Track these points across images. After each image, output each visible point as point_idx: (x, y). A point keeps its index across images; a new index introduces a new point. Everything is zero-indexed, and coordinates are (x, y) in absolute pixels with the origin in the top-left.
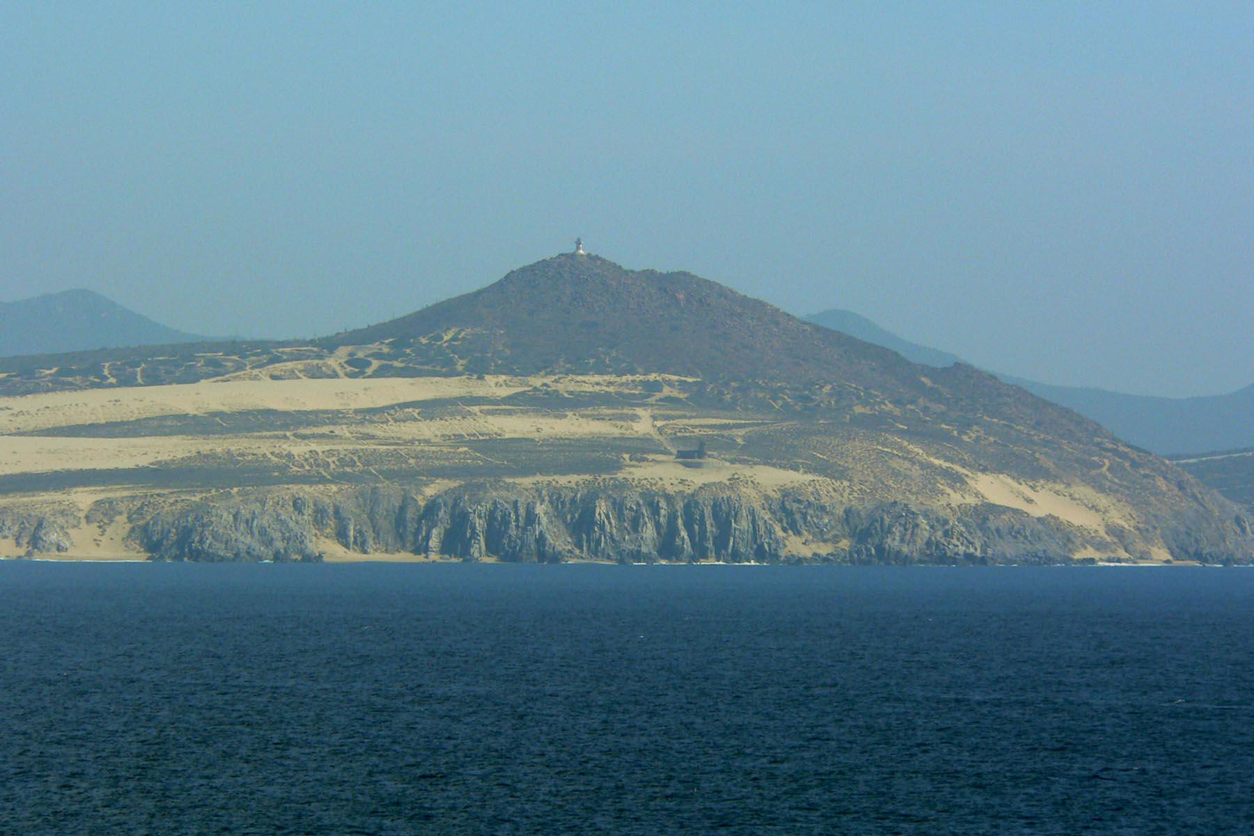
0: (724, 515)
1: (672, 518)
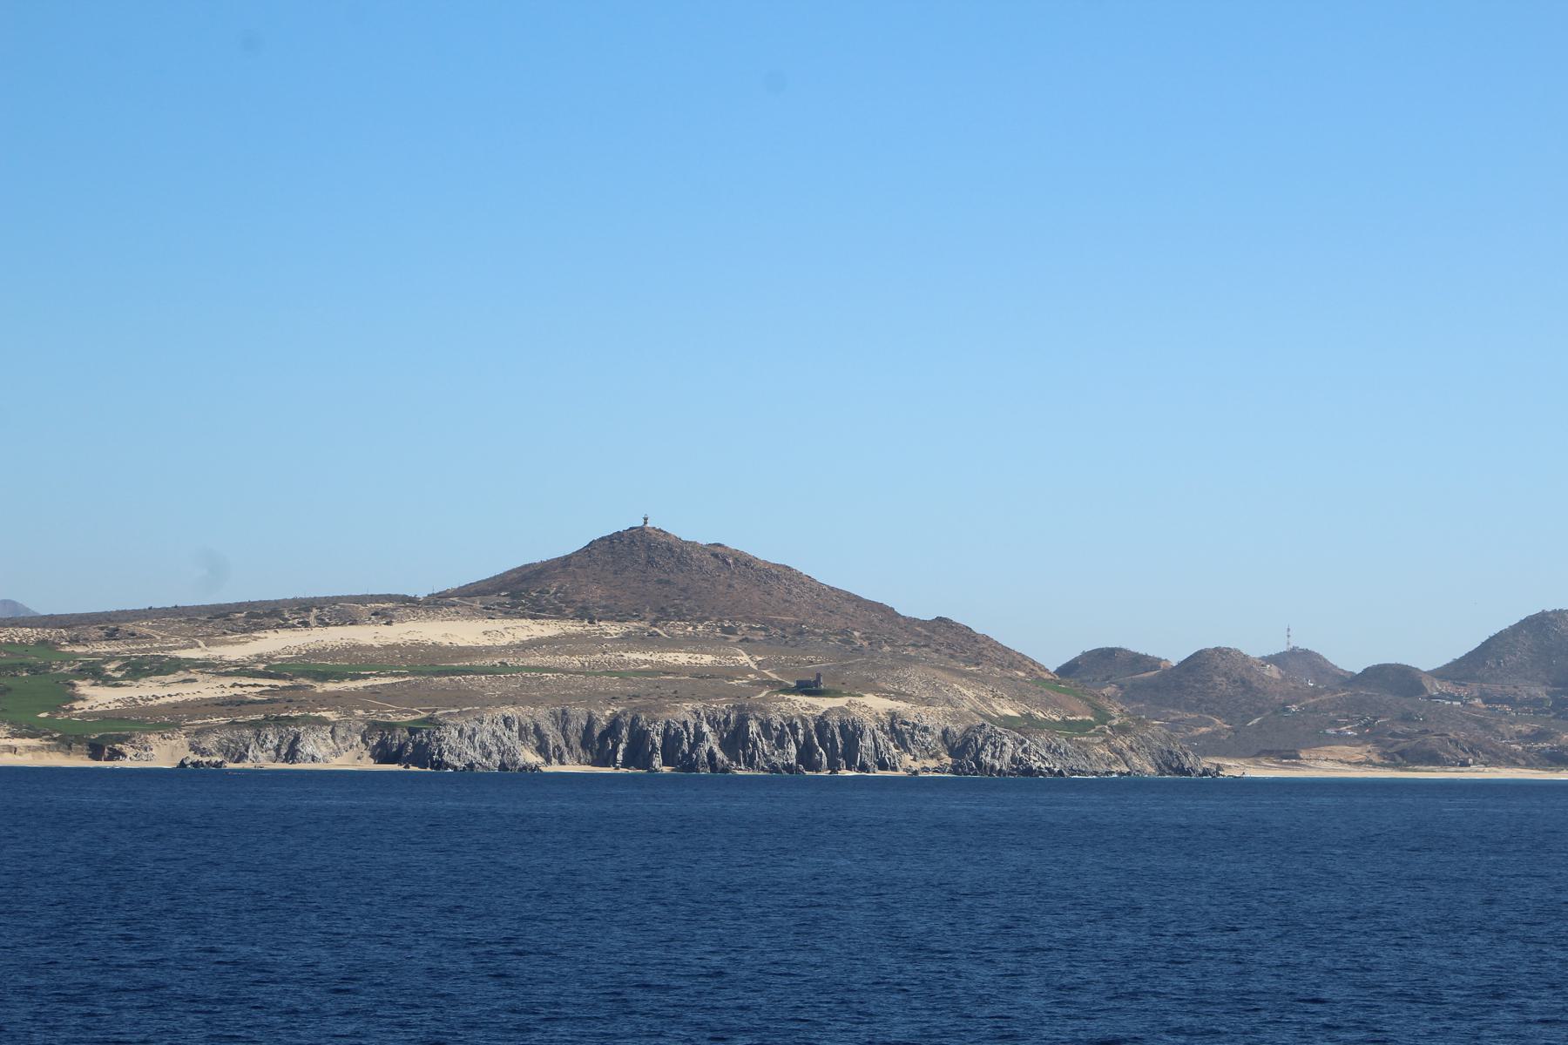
0: (852, 734)
1: (808, 735)
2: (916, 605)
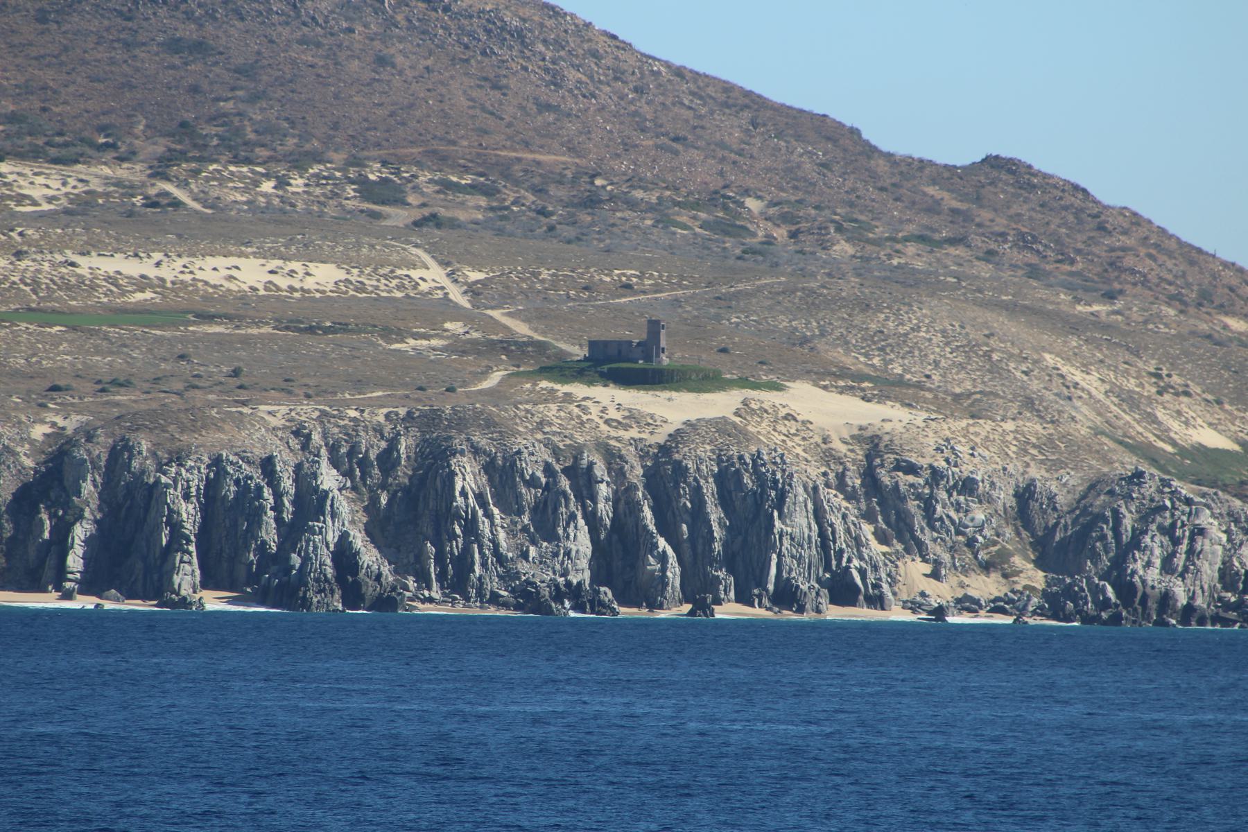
0: (753, 498)
1: (624, 501)
2: (927, 119)
